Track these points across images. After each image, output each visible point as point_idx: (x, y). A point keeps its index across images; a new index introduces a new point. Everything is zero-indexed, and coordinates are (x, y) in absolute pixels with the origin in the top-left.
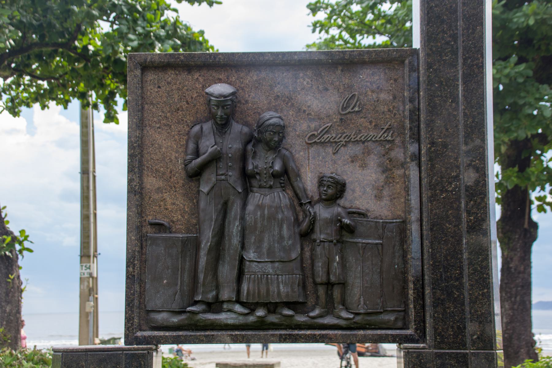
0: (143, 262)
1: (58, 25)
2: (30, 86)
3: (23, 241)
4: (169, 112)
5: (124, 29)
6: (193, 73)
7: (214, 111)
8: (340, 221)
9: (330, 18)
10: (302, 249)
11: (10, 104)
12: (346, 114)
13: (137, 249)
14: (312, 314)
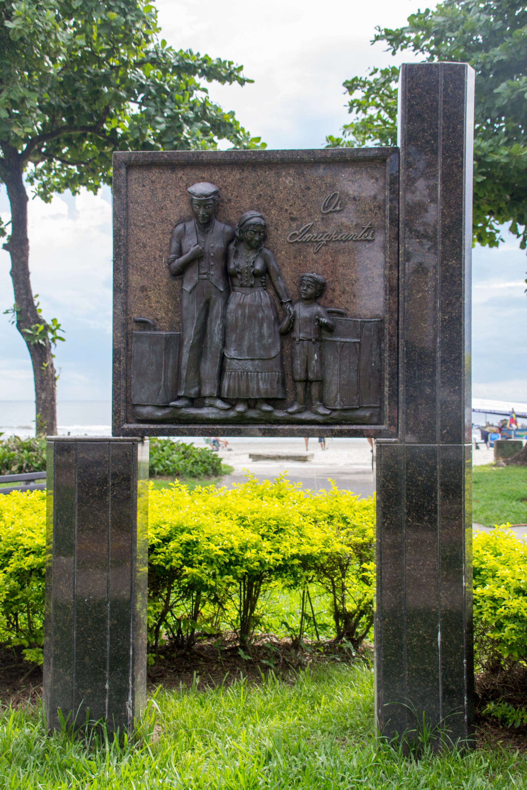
0: (129, 358)
1: (86, 108)
2: (61, 170)
3: (55, 329)
4: (153, 211)
5: (152, 111)
6: (177, 171)
7: (196, 210)
8: (318, 320)
9: (367, 97)
10: (282, 347)
11: (42, 190)
12: (327, 213)
13: (123, 345)
14: (290, 410)
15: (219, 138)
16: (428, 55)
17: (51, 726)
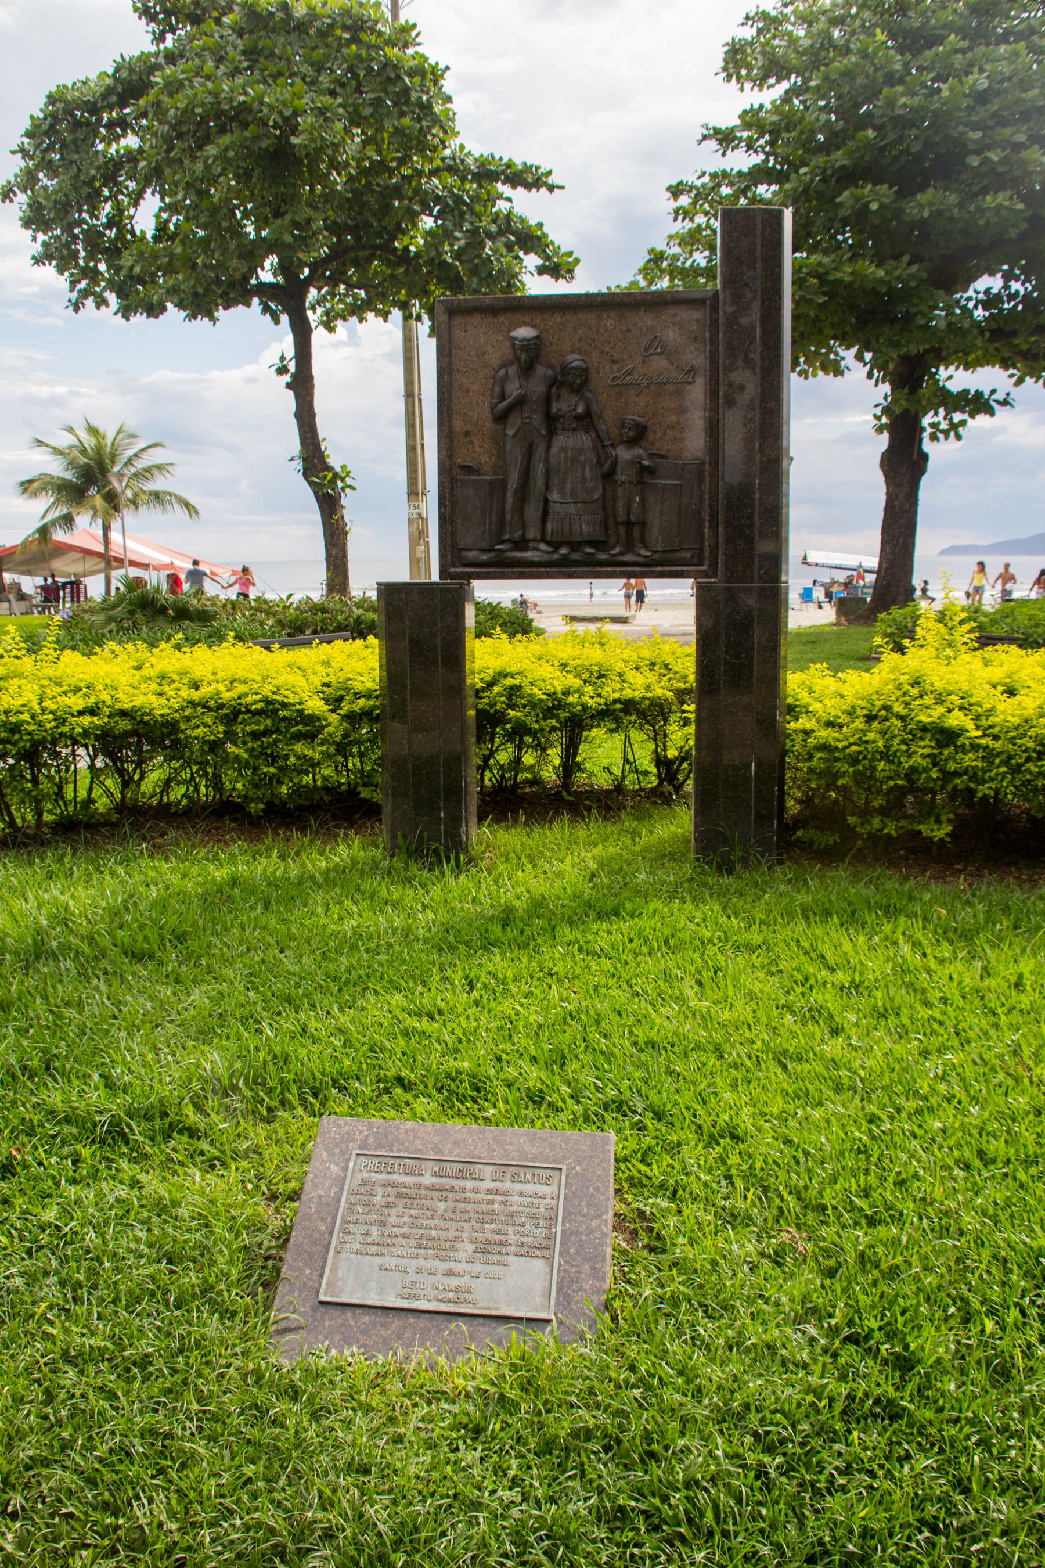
2: (346, 295)
5: (449, 225)
10: (604, 490)
15: (526, 253)
16: (762, 157)
17: (392, 849)
